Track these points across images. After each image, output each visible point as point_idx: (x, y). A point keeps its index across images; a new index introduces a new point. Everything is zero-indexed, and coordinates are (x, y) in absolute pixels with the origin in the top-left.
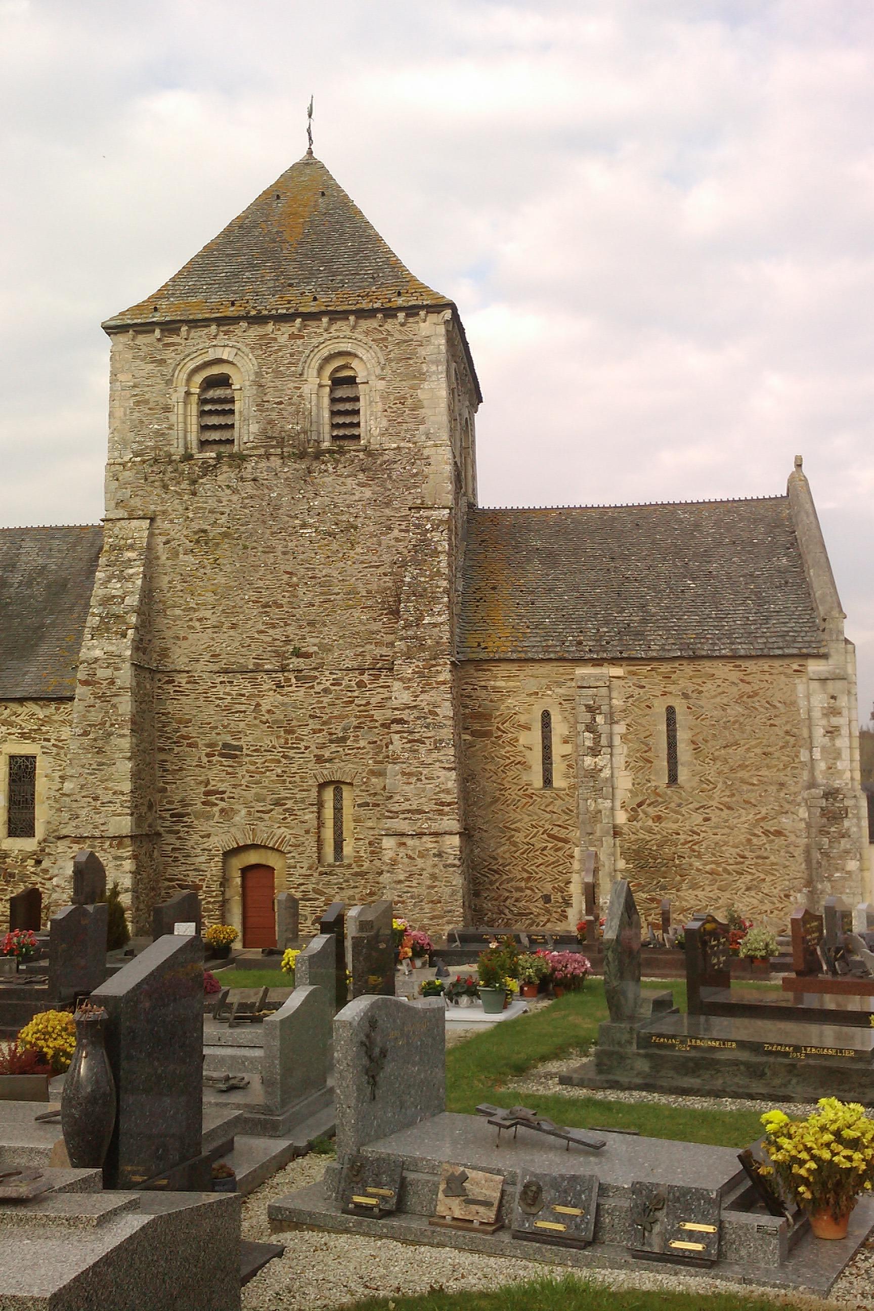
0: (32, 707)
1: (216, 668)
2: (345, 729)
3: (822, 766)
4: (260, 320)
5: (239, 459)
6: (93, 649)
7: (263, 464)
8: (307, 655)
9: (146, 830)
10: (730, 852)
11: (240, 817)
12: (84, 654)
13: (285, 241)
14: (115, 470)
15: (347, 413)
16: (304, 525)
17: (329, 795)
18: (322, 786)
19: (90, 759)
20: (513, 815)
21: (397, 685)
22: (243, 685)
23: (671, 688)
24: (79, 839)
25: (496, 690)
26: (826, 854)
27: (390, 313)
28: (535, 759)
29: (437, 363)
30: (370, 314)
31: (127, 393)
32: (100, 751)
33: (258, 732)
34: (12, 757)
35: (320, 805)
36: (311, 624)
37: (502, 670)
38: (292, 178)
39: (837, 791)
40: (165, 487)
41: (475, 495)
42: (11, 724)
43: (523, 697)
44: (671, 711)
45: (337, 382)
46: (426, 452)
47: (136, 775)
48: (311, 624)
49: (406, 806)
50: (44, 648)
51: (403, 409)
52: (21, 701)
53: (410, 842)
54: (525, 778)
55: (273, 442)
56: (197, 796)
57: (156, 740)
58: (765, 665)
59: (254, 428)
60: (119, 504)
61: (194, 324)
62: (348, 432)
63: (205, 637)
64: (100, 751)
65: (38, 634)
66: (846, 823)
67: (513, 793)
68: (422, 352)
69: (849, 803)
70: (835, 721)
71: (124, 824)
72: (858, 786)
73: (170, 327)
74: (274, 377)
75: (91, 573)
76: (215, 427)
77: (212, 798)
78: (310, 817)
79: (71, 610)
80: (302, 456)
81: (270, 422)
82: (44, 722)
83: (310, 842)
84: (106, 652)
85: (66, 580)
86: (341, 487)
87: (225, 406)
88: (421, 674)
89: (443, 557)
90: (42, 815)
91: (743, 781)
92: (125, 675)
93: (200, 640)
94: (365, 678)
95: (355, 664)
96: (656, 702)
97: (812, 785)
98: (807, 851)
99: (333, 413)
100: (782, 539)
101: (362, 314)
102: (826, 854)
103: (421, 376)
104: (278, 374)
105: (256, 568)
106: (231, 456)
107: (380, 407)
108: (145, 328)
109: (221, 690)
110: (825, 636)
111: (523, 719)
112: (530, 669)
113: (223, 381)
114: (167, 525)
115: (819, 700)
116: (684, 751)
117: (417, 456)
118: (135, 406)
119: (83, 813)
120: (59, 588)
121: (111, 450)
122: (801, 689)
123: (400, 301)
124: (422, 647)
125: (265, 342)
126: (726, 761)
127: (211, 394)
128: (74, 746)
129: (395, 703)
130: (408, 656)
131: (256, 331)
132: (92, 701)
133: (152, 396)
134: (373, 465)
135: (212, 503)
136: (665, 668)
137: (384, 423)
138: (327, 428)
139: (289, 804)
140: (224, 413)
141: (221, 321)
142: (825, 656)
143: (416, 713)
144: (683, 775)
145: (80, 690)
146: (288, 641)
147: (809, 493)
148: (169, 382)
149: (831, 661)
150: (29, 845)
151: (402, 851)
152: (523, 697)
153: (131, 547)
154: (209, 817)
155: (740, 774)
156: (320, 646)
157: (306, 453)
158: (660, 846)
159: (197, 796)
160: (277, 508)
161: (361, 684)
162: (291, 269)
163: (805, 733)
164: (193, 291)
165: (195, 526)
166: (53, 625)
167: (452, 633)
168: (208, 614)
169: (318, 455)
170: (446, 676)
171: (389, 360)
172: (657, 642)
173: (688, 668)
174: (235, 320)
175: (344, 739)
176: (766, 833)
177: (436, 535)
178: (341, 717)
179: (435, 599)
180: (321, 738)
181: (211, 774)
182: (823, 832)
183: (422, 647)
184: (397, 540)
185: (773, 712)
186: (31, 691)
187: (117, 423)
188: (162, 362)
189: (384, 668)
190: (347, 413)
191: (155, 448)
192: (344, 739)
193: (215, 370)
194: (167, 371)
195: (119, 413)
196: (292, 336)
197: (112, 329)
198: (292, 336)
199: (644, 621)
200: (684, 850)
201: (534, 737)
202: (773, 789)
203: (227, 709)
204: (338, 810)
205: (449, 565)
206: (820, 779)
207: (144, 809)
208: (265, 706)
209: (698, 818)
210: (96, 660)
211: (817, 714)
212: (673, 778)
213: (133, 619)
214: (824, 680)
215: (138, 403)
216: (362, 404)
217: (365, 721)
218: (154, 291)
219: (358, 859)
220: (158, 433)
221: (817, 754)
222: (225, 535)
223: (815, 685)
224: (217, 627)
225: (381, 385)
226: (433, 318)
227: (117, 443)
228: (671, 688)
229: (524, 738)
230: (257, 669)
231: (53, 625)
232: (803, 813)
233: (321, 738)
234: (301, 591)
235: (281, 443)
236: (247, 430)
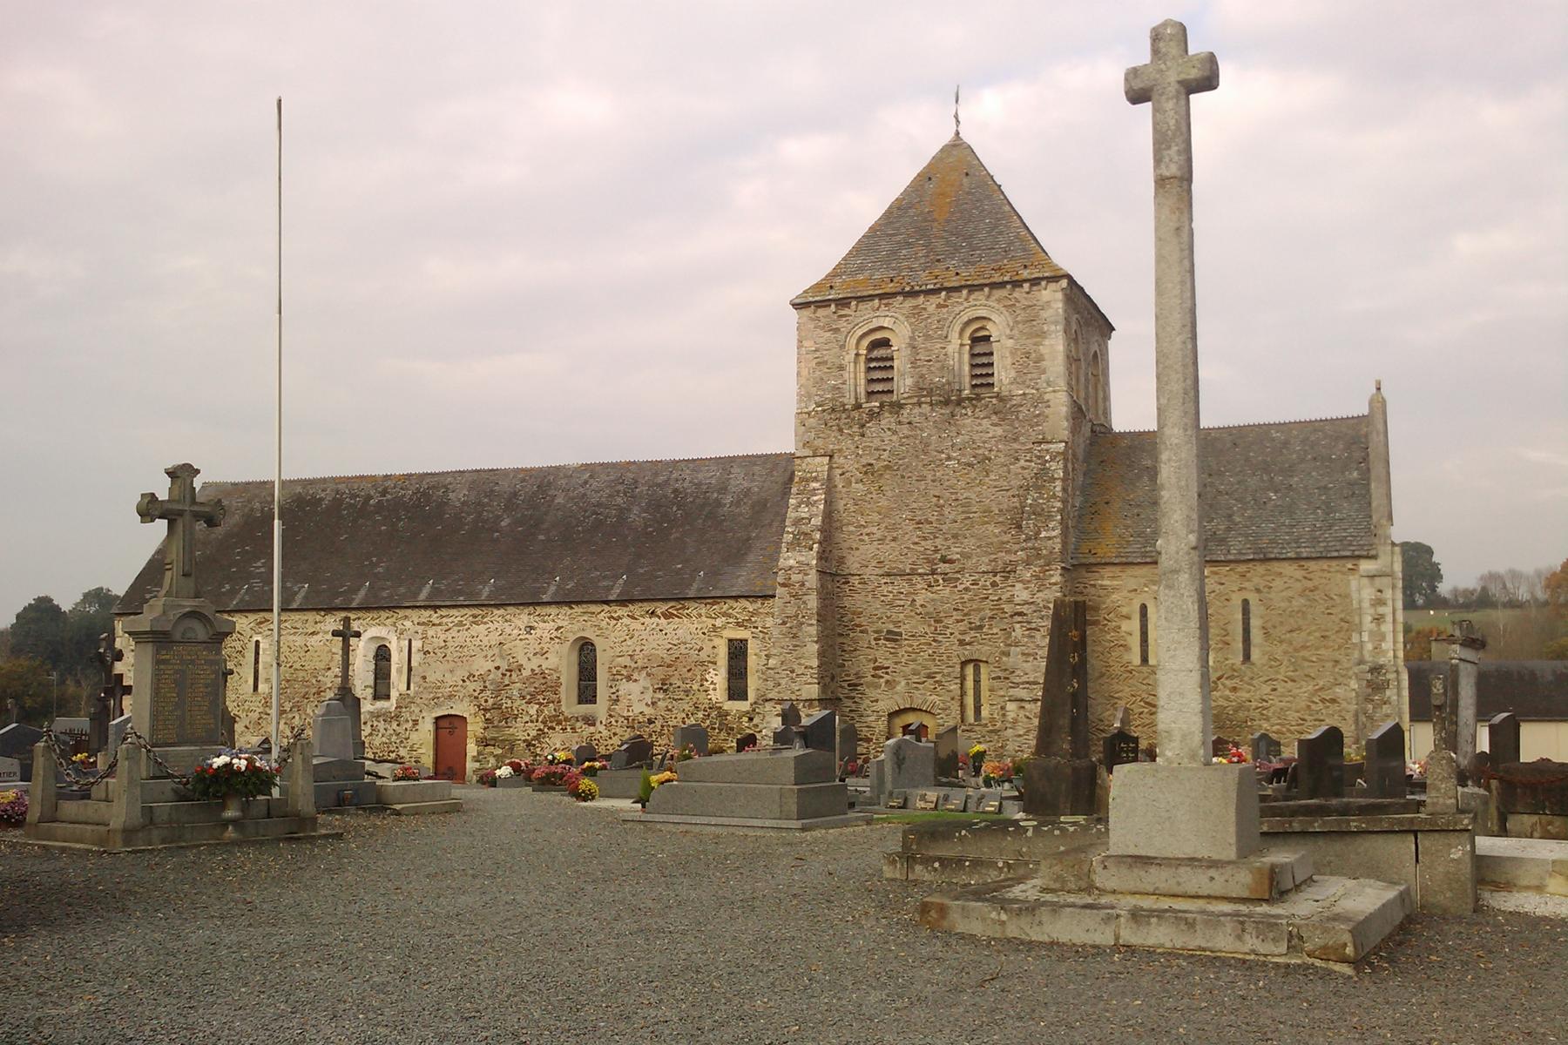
0: (744, 603)
1: (880, 572)
2: (982, 619)
3: (1369, 646)
4: (913, 294)
5: (897, 407)
6: (789, 559)
7: (917, 410)
8: (951, 562)
9: (829, 695)
10: (1292, 716)
11: (901, 687)
12: (782, 563)
13: (934, 220)
14: (802, 417)
15: (984, 365)
16: (949, 458)
17: (970, 670)
18: (964, 664)
19: (787, 641)
20: (1116, 687)
21: (1019, 586)
22: (902, 585)
23: (1246, 585)
24: (780, 701)
25: (1103, 587)
26: (1370, 718)
27: (1017, 284)
28: (1135, 642)
29: (1056, 323)
30: (1002, 285)
31: (810, 356)
32: (795, 636)
33: (914, 622)
34: (730, 640)
35: (963, 678)
36: (955, 536)
37: (1107, 572)
38: (941, 159)
39: (1382, 667)
40: (841, 430)
41: (1106, 413)
42: (729, 616)
43: (1125, 593)
44: (1246, 603)
45: (975, 340)
46: (1047, 397)
47: (821, 654)
48: (955, 536)
49: (1025, 679)
50: (751, 557)
51: (1029, 362)
52: (736, 598)
53: (1027, 706)
54: (1126, 657)
55: (924, 391)
56: (868, 670)
57: (836, 628)
58: (1324, 564)
59: (909, 381)
60: (806, 444)
61: (861, 299)
62: (984, 381)
63: (872, 548)
64: (795, 636)
65: (745, 546)
66: (1388, 693)
67: (1117, 669)
68: (1044, 314)
69: (1391, 676)
70: (1381, 610)
71: (813, 691)
72: (1401, 662)
73: (842, 303)
74: (923, 339)
75: (786, 493)
76: (879, 380)
77: (880, 672)
78: (955, 687)
79: (770, 525)
80: (947, 403)
81: (922, 376)
82: (753, 614)
83: (955, 706)
84: (798, 561)
85: (766, 500)
86: (978, 427)
87: (886, 364)
88: (1038, 578)
89: (1058, 483)
90: (753, 683)
91: (1305, 659)
92: (812, 579)
93: (868, 550)
94: (998, 579)
95: (990, 568)
96: (1234, 596)
97: (1361, 662)
98: (1356, 715)
99: (973, 366)
100: (1357, 455)
101: (994, 286)
102: (1370, 718)
103: (1043, 335)
104: (927, 337)
105: (911, 492)
106: (892, 404)
107: (1009, 361)
108: (824, 304)
109: (885, 589)
110: (1376, 541)
111: (1124, 611)
112: (1130, 571)
113: (885, 343)
114: (842, 460)
115: (1368, 593)
116: (1256, 636)
117: (1039, 401)
118: (818, 366)
119: (783, 682)
120: (761, 506)
121: (799, 401)
122: (1354, 584)
123: (1025, 274)
124: (1038, 556)
125: (917, 312)
126: (1291, 643)
127: (876, 354)
128: (775, 633)
129: (1017, 600)
130: (1028, 563)
131: (911, 302)
132: (788, 598)
133: (830, 357)
134: (1003, 409)
135: (877, 443)
136: (1242, 568)
137: (1013, 374)
138: (967, 379)
139: (938, 677)
140: (885, 368)
141: (881, 297)
142: (1374, 557)
143: (1033, 607)
144: (1255, 654)
145: (780, 591)
146: (936, 551)
147: (1385, 413)
148: (842, 347)
149: (1379, 561)
150: (744, 706)
151: (1022, 713)
152: (1125, 593)
153: (815, 479)
154: (878, 686)
155: (1305, 653)
156: (961, 554)
157: (950, 400)
158: (1236, 711)
159: (868, 670)
160: (927, 445)
161: (994, 584)
162: (939, 245)
163: (1357, 620)
164: (861, 269)
165: (864, 461)
166: (757, 538)
167: (1064, 544)
168: (874, 530)
169: (959, 403)
170: (1057, 578)
171: (1017, 323)
172: (1236, 545)
173: (1260, 569)
174: (894, 295)
175: (981, 627)
176: (1323, 700)
177: (1053, 465)
178: (979, 610)
179: (1050, 517)
180: (963, 626)
181: (878, 654)
182: (1368, 699)
183: (1038, 556)
184: (1023, 468)
185: (1330, 603)
186: (744, 590)
187: (803, 381)
188: (837, 330)
189: (1008, 571)
190: (984, 365)
191: (832, 400)
192: (981, 627)
193: (878, 335)
194: (841, 337)
195: (805, 372)
196: (939, 306)
197: (797, 306)
198: (939, 306)
199: (1229, 529)
200: (1256, 714)
201: (1134, 625)
202: (1329, 665)
203: (890, 604)
204: (977, 682)
205: (1064, 490)
206: (1367, 657)
207: (828, 680)
208: (919, 600)
209: (1267, 689)
210: (791, 568)
211: (1366, 604)
212: (1247, 657)
213: (818, 536)
214: (1372, 577)
215: (818, 364)
216: (995, 358)
217: (997, 613)
218: (829, 270)
219: (992, 720)
220: (835, 388)
221: (1365, 637)
222: (887, 467)
223: (1365, 581)
224: (882, 540)
225: (1010, 343)
226: (1052, 286)
227: (804, 396)
228: (1246, 585)
229: (1125, 626)
230: (913, 573)
231: (757, 538)
232: (1354, 684)
233: (963, 626)
234: (946, 510)
235: (930, 393)
236: (903, 383)
